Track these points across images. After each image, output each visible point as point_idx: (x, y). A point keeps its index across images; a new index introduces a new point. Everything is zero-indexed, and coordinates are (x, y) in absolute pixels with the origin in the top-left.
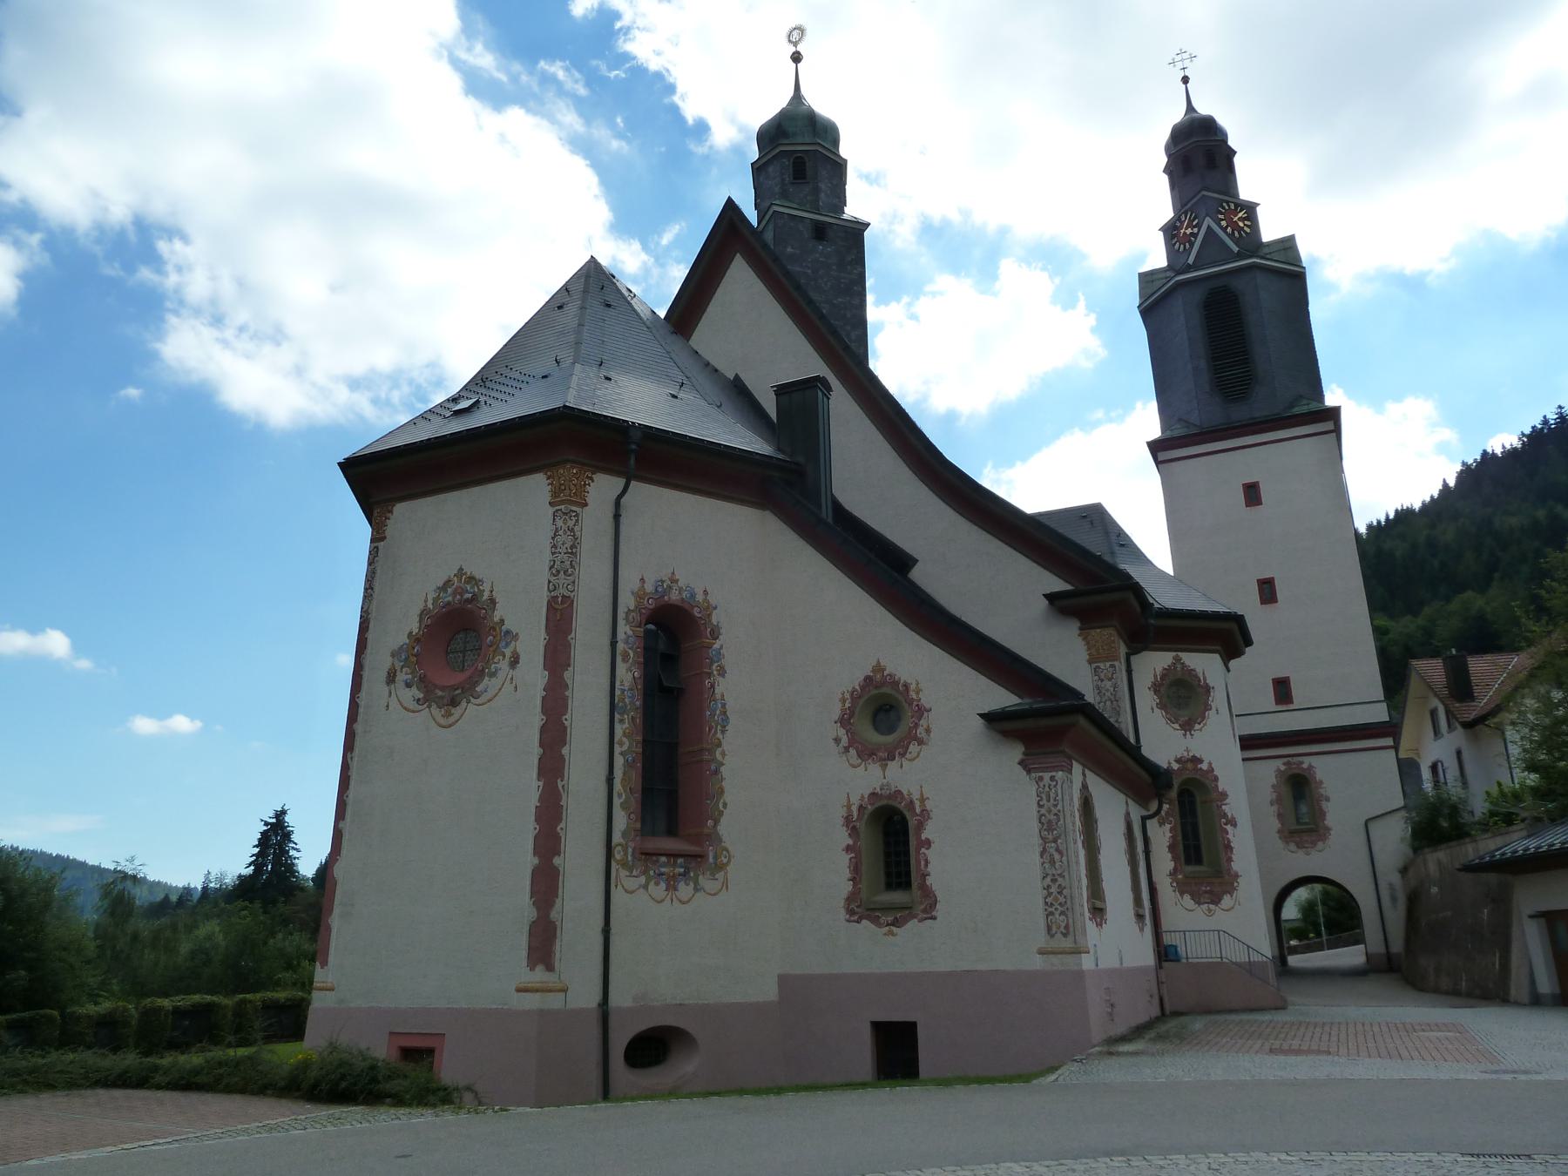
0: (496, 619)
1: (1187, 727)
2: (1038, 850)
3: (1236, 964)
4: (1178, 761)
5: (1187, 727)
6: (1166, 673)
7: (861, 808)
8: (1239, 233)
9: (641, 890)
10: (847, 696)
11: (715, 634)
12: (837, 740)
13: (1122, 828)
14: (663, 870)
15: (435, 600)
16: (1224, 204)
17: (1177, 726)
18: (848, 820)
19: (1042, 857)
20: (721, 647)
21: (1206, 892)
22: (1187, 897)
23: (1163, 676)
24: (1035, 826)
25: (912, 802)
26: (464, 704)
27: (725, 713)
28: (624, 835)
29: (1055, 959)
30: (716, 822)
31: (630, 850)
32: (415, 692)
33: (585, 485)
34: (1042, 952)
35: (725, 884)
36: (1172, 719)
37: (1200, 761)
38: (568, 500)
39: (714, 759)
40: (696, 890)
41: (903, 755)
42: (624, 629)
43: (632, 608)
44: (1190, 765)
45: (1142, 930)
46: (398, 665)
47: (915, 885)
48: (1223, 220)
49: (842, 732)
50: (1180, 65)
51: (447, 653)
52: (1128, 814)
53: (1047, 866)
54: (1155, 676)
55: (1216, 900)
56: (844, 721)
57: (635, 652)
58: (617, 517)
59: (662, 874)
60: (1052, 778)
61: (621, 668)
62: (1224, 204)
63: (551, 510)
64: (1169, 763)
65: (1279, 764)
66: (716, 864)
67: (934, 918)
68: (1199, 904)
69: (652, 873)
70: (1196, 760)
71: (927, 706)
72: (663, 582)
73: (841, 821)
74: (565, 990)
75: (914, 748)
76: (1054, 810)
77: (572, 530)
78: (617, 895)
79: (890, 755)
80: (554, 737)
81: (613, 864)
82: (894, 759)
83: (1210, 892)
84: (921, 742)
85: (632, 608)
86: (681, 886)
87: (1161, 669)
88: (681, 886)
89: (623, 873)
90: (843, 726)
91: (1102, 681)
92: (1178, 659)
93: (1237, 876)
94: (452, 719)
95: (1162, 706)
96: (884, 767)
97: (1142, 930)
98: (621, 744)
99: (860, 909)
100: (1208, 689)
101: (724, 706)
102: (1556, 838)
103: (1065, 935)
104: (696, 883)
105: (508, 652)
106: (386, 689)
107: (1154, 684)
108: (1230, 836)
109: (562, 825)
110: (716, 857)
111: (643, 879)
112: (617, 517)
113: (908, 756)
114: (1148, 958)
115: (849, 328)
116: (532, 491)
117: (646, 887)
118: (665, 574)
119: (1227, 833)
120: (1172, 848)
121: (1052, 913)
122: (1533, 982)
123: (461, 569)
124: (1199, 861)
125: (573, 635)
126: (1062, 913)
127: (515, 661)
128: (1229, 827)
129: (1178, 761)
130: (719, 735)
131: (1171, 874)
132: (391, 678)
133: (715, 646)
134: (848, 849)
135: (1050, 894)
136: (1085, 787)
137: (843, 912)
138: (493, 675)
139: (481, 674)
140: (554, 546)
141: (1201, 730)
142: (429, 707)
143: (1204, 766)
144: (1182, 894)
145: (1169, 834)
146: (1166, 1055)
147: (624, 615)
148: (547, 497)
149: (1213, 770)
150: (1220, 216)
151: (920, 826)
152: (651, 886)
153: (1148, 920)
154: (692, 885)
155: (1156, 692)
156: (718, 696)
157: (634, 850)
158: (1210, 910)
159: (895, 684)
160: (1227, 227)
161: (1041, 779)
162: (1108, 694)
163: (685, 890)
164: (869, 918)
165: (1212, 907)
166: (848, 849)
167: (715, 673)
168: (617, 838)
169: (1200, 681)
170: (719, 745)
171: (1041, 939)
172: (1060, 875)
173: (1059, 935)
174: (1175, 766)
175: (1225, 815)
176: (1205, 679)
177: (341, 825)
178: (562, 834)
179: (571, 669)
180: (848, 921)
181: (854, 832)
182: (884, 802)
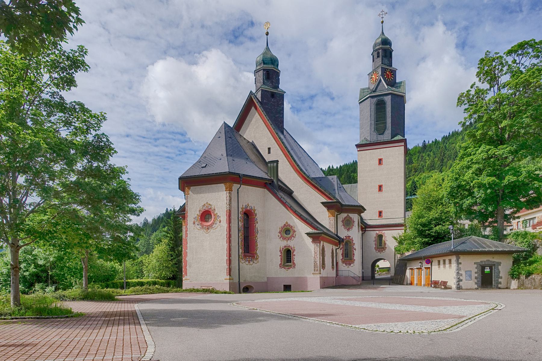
0: (216, 213)
1: (348, 230)
4: (346, 237)
5: (348, 230)
6: (345, 218)
12: (279, 236)
13: (331, 251)
15: (202, 208)
16: (387, 70)
22: (344, 264)
26: (210, 229)
27: (258, 231)
28: (241, 253)
30: (256, 251)
35: (258, 262)
37: (350, 237)
38: (230, 190)
39: (256, 239)
42: (240, 215)
45: (333, 270)
46: (195, 221)
49: (279, 235)
50: (381, 16)
52: (333, 249)
58: (238, 193)
62: (387, 70)
75: (293, 238)
78: (240, 264)
79: (289, 239)
84: (294, 237)
89: (241, 260)
92: (348, 215)
94: (208, 232)
95: (344, 225)
97: (333, 270)
99: (282, 266)
102: (1, 340)
105: (219, 220)
111: (244, 261)
112: (238, 193)
114: (335, 276)
117: (245, 262)
118: (247, 204)
120: (342, 254)
122: (407, 281)
124: (348, 257)
127: (220, 222)
128: (354, 250)
129: (346, 237)
132: (194, 223)
136: (323, 245)
143: (351, 238)
144: (343, 263)
146: (188, 136)
151: (293, 252)
153: (335, 268)
159: (290, 226)
164: (284, 268)
166: (280, 256)
171: (313, 271)
174: (345, 238)
177: (230, 258)
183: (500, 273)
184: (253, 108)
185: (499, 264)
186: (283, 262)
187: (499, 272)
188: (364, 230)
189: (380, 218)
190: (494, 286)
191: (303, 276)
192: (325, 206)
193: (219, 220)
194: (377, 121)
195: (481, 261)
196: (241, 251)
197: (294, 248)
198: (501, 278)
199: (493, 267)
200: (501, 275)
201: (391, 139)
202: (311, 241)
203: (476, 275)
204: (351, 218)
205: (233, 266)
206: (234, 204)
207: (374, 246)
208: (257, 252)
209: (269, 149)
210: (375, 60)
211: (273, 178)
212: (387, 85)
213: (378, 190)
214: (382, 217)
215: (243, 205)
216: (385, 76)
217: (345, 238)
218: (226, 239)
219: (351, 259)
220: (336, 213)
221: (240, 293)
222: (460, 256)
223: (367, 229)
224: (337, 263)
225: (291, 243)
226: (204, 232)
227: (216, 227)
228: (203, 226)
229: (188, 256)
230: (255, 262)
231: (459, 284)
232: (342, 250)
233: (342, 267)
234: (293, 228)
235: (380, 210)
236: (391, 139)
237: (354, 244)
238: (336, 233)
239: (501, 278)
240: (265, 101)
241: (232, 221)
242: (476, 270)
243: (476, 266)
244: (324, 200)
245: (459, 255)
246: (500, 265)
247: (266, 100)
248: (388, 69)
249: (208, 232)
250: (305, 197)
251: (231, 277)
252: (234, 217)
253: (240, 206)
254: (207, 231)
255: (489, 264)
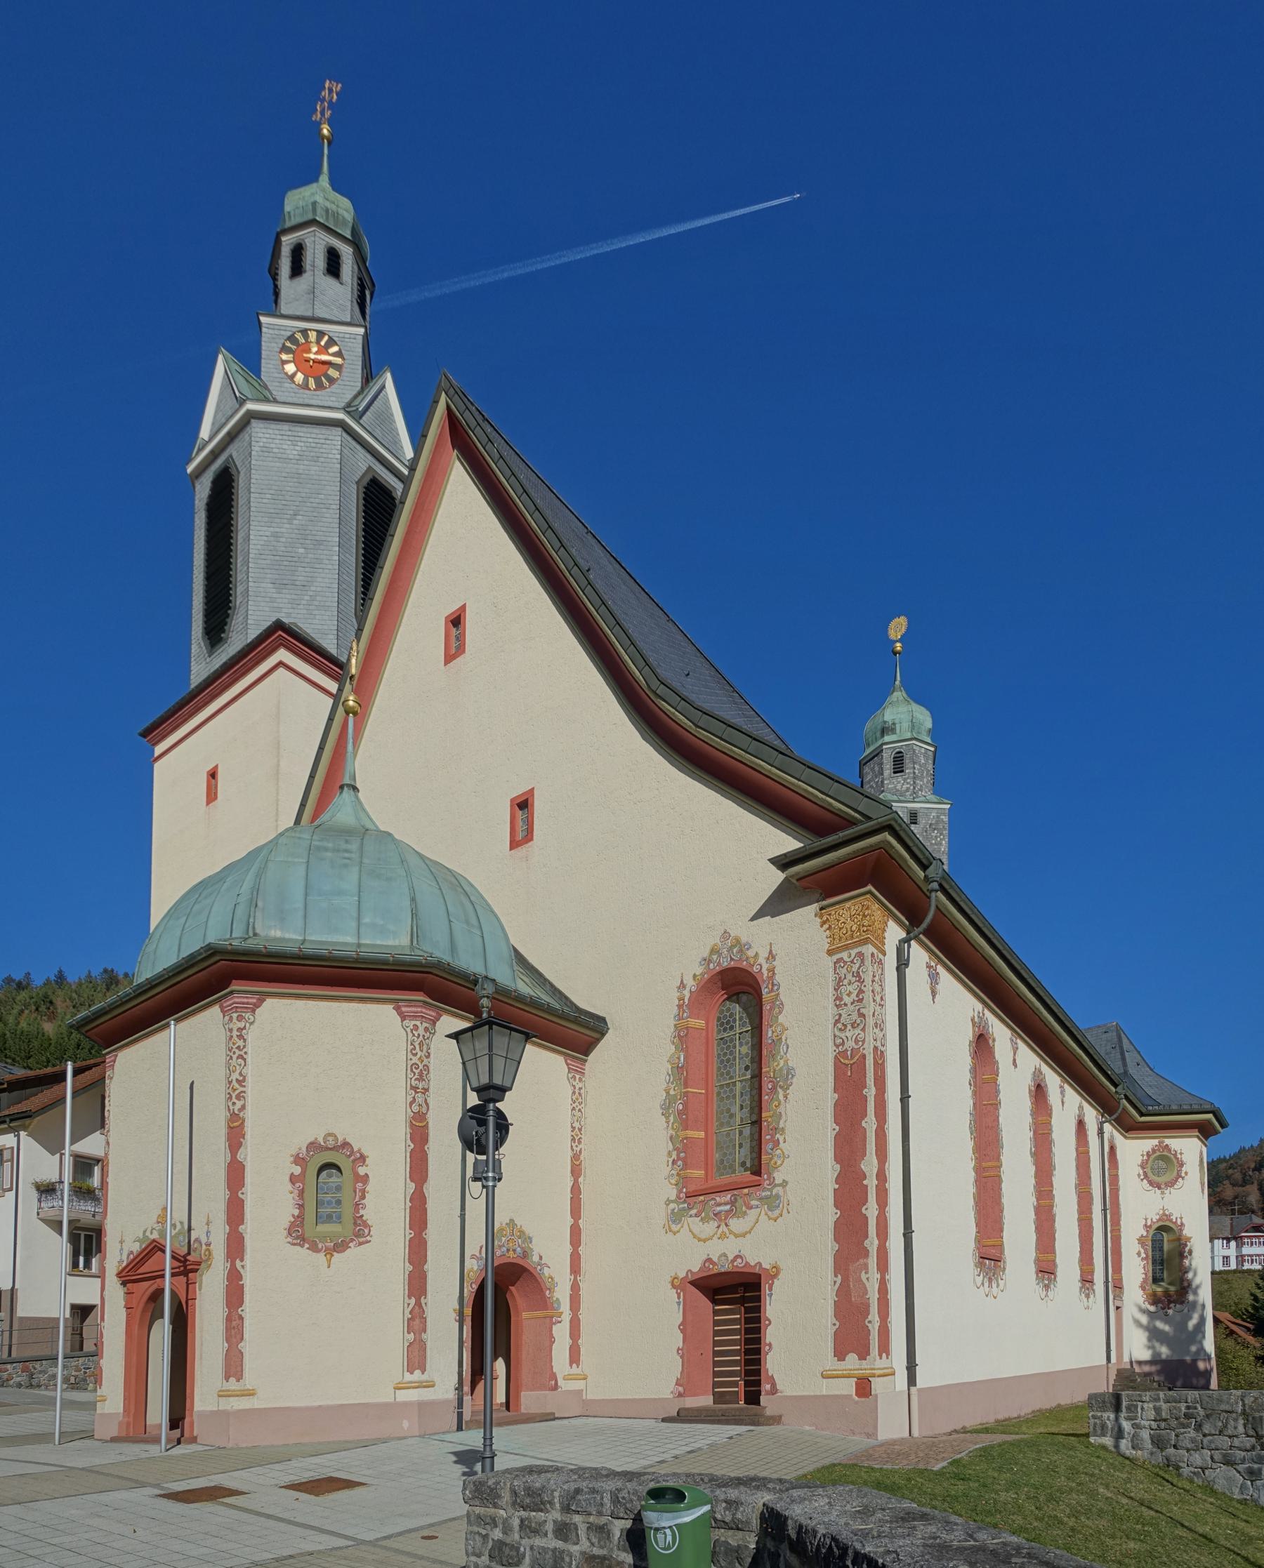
16: (299, 336)
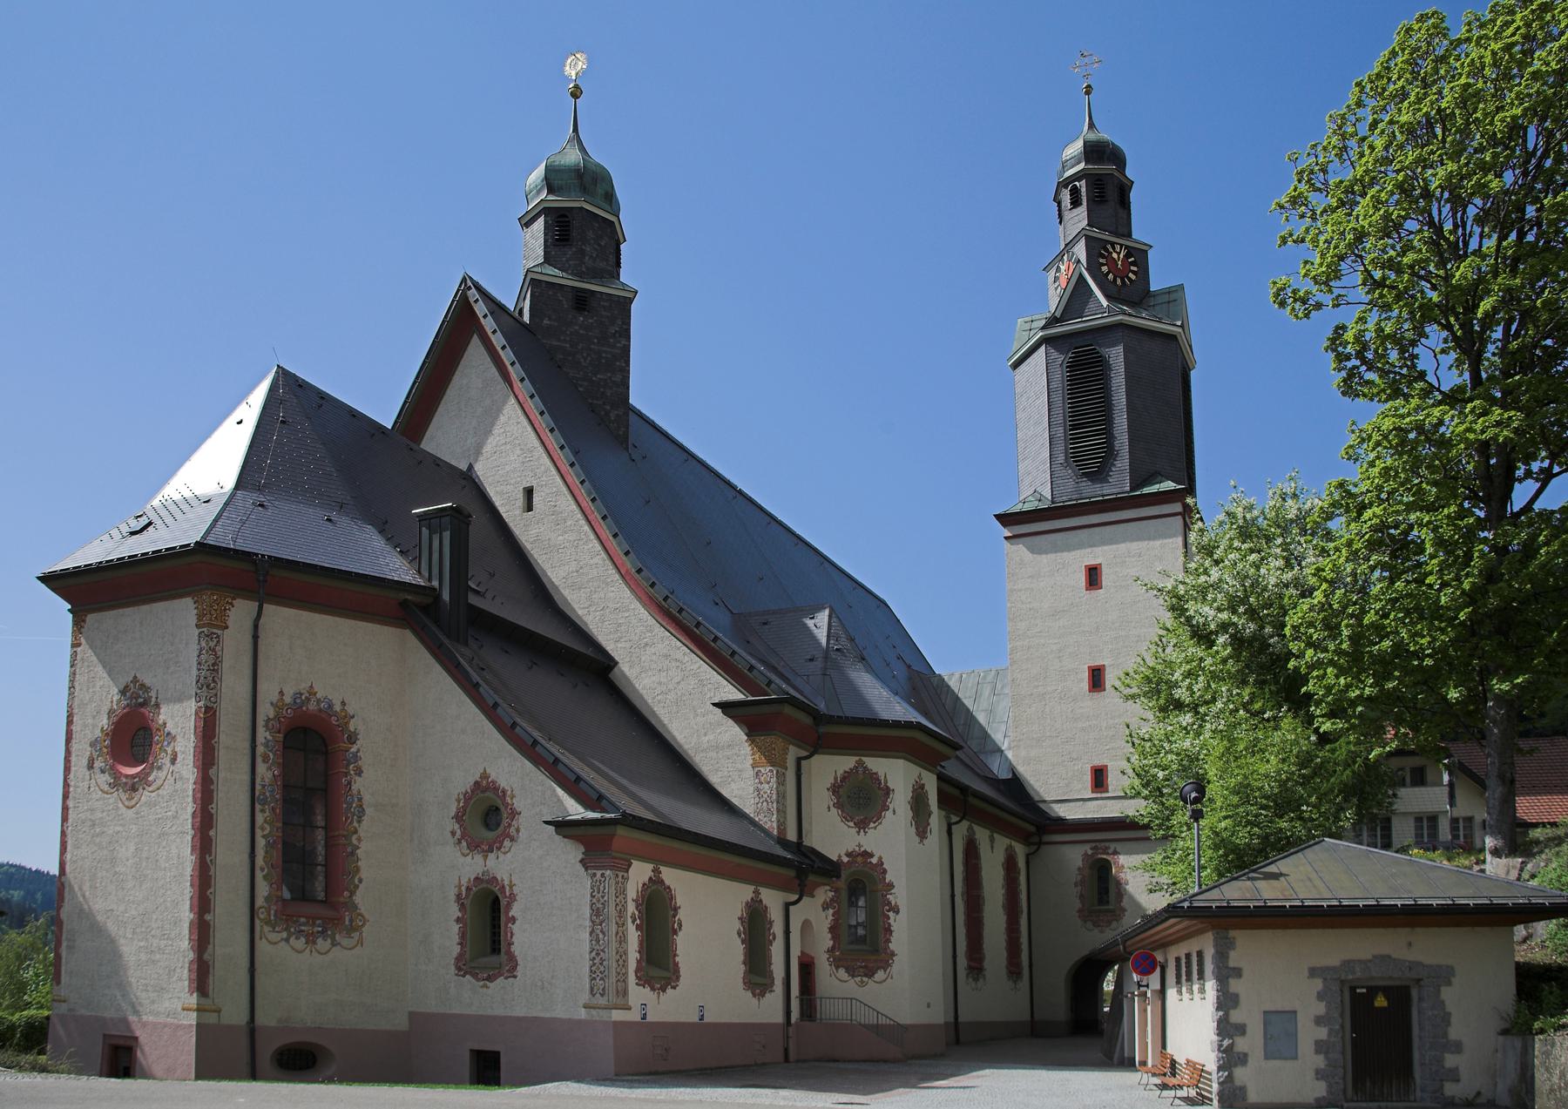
0: (161, 722)
1: (862, 826)
2: (588, 930)
3: (865, 1026)
4: (848, 855)
5: (862, 826)
6: (847, 776)
7: (468, 889)
8: (1123, 281)
9: (283, 943)
10: (462, 797)
11: (353, 738)
12: (453, 833)
14: (303, 928)
16: (1109, 247)
17: (852, 824)
18: (459, 896)
19: (591, 935)
20: (358, 751)
21: (861, 967)
23: (844, 779)
24: (588, 912)
25: (503, 887)
26: (141, 790)
28: (267, 899)
29: (594, 1012)
30: (352, 893)
31: (272, 912)
32: (106, 778)
33: (225, 609)
34: (585, 1007)
35: (360, 942)
36: (846, 817)
37: (872, 855)
39: (351, 844)
40: (333, 945)
41: (499, 849)
42: (262, 735)
43: (271, 716)
44: (859, 859)
47: (503, 950)
48: (1104, 265)
49: (457, 826)
51: (132, 747)
53: (594, 942)
54: (836, 778)
55: (870, 974)
56: (458, 818)
57: (275, 755)
58: (256, 637)
59: (303, 931)
60: (603, 875)
61: (261, 768)
62: (1109, 247)
63: (197, 632)
64: (840, 856)
65: (1087, 848)
66: (351, 925)
67: (515, 977)
68: (853, 976)
69: (292, 930)
70: (867, 855)
71: (518, 810)
72: (301, 694)
73: (453, 898)
74: (219, 1011)
75: (507, 843)
76: (602, 901)
77: (214, 650)
78: (262, 946)
80: (205, 822)
81: (257, 922)
82: (492, 852)
83: (866, 967)
84: (512, 839)
85: (271, 716)
86: (320, 941)
87: (842, 772)
88: (320, 941)
89: (266, 929)
90: (458, 822)
91: (762, 783)
92: (860, 763)
93: (893, 954)
94: (133, 802)
95: (838, 805)
96: (486, 857)
98: (263, 829)
99: (465, 966)
100: (888, 791)
101: (360, 800)
103: (602, 995)
104: (333, 939)
105: (169, 750)
106: (88, 773)
107: (833, 785)
108: (891, 921)
109: (212, 890)
110: (351, 921)
111: (285, 935)
112: (256, 637)
113: (503, 850)
115: (608, 408)
116: (181, 614)
117: (287, 940)
118: (304, 686)
119: (889, 918)
121: (594, 979)
123: (135, 677)
125: (216, 739)
126: (602, 979)
128: (891, 914)
129: (848, 855)
130: (355, 824)
131: (828, 951)
132: (90, 766)
133: (352, 750)
134: (458, 920)
135: (594, 964)
137: (453, 968)
138: (160, 768)
139: (152, 768)
140: (199, 664)
141: (875, 828)
142: (118, 790)
144: (837, 968)
145: (831, 918)
147: (263, 723)
148: (193, 620)
149: (882, 864)
150: (1101, 260)
151: (509, 906)
152: (292, 940)
154: (329, 941)
155: (834, 792)
156: (355, 792)
157: (276, 911)
158: (862, 982)
159: (496, 789)
160: (1108, 273)
161: (595, 875)
162: (765, 796)
163: (322, 944)
165: (865, 979)
166: (458, 920)
167: (352, 772)
168: (260, 902)
169: (880, 783)
170: (356, 832)
171: (585, 997)
172: (603, 951)
173: (598, 995)
175: (889, 903)
176: (886, 782)
178: (212, 897)
179: (215, 767)
180: (456, 975)
181: (462, 907)
182: (485, 885)
183: (1449, 1024)
184: (475, 340)
185: (1444, 975)
186: (467, 949)
187: (1446, 1019)
188: (1036, 839)
189: (1099, 795)
190: (1423, 1090)
191: (548, 1015)
192: (738, 720)
193: (169, 752)
194: (1074, 427)
195: (1347, 964)
196: (263, 889)
197: (511, 887)
198: (1457, 1047)
199: (1414, 993)
200: (1454, 1033)
201: (1132, 490)
202: (581, 856)
203: (1322, 1033)
204: (874, 777)
205: (219, 951)
206: (234, 686)
207: (1078, 905)
208: (358, 898)
209: (529, 492)
210: (1067, 215)
211: (435, 583)
212: (1107, 297)
213: (1085, 685)
214: (1107, 791)
215: (281, 693)
216: (1105, 269)
217: (845, 859)
218: (191, 832)
219: (876, 951)
220: (793, 752)
221: (254, 1075)
222: (1232, 933)
223: (1047, 838)
224: (807, 968)
225: (503, 866)
226: (120, 805)
227: (159, 782)
228: (117, 776)
229: (66, 900)
230: (345, 942)
231: (1230, 1078)
232: (831, 911)
233: (833, 983)
234: (508, 800)
235: (1098, 762)
236: (1132, 490)
237: (891, 886)
238: (792, 836)
239: (1457, 1047)
240: (546, 322)
241: (222, 755)
242: (1321, 1008)
243: (1318, 984)
244: (733, 694)
245: (1227, 929)
246: (1449, 983)
247: (550, 319)
248: (1113, 244)
249: (133, 802)
250: (660, 683)
251: (207, 1002)
252: (232, 737)
253: (268, 693)
254: (130, 799)
255: (1391, 978)
